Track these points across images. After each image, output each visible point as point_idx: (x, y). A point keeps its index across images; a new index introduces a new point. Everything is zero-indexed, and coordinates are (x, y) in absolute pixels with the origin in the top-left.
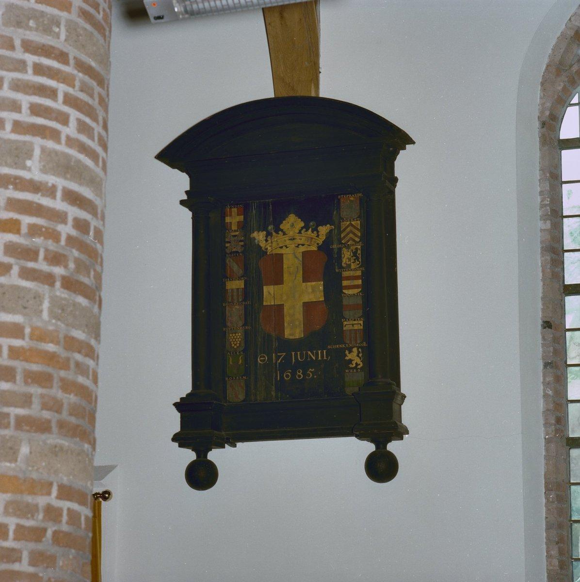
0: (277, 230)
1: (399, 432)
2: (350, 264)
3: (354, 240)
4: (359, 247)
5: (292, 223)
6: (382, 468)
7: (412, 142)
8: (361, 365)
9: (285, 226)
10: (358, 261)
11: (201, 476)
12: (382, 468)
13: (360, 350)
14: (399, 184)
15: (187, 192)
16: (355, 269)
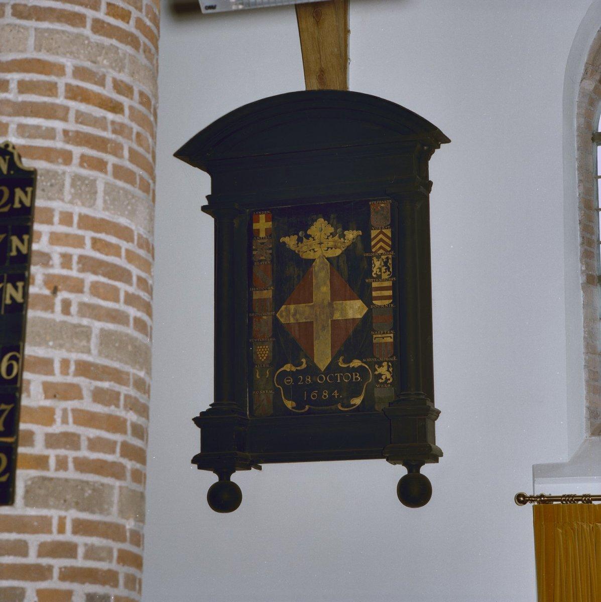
0: (308, 237)
1: (434, 456)
2: (381, 274)
3: (384, 249)
4: (390, 256)
5: (320, 228)
6: (414, 492)
7: (448, 141)
8: (391, 380)
9: (313, 230)
10: (389, 271)
11: (224, 498)
12: (414, 492)
13: (390, 364)
14: (434, 188)
15: (208, 197)
16: (387, 280)
